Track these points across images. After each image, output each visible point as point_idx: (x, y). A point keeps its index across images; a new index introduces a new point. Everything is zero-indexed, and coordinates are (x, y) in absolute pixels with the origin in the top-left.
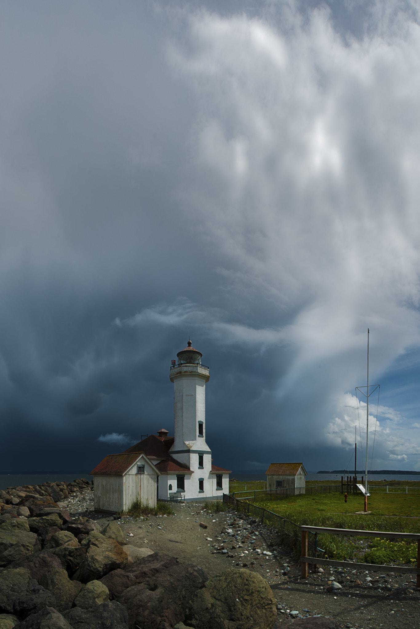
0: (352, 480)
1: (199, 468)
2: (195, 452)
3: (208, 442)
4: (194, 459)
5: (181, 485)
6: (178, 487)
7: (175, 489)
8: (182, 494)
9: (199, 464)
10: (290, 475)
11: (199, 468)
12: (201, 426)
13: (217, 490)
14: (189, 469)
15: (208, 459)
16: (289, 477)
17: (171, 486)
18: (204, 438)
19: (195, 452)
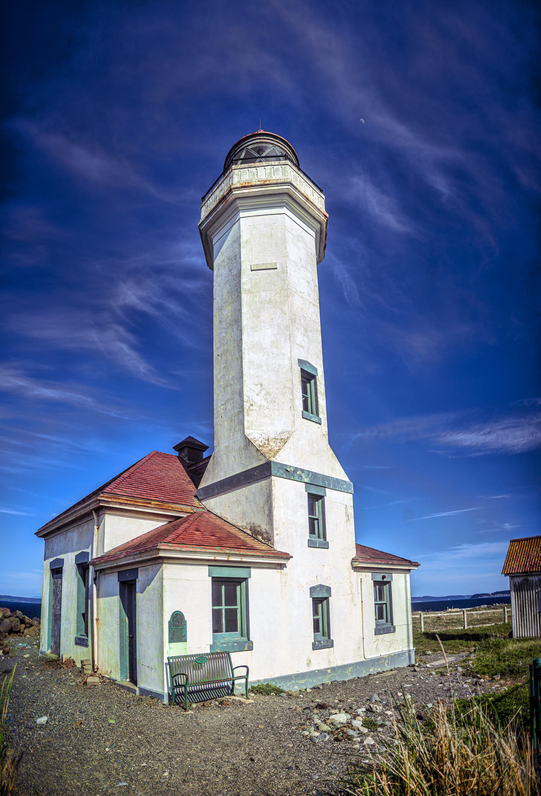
1: (311, 544)
2: (289, 473)
3: (335, 442)
6: (217, 629)
8: (237, 658)
11: (311, 544)
12: (307, 377)
15: (339, 505)
19: (289, 473)
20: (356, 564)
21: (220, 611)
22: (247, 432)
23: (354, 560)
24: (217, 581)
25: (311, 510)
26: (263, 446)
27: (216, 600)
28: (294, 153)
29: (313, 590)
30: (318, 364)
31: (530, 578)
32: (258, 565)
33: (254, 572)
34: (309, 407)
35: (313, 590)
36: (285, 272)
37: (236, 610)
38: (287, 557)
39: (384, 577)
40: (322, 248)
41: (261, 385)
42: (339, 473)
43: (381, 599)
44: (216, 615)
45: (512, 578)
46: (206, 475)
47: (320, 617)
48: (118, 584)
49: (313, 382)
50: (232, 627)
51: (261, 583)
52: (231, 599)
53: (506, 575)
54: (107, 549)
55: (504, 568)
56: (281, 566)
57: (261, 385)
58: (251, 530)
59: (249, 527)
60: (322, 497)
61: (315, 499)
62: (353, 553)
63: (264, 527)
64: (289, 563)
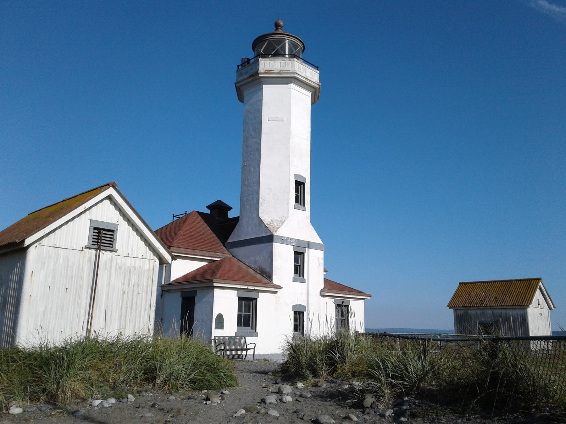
0: (97, 231)
1: (294, 280)
2: (284, 241)
3: (315, 221)
4: (282, 258)
5: (247, 316)
6: (239, 324)
7: (231, 328)
8: (249, 340)
9: (296, 272)
10: (513, 307)
11: (294, 280)
12: (299, 185)
13: (230, 208)
14: (269, 276)
15: (315, 260)
16: (500, 311)
17: (220, 318)
18: (308, 212)
19: (284, 241)
20: (323, 293)
21: (242, 315)
22: (260, 216)
23: (322, 290)
24: (241, 299)
25: (296, 260)
26: (270, 225)
27: (240, 309)
28: (301, 42)
29: (294, 307)
30: (306, 175)
31: (469, 312)
32: (273, 80)
33: (261, 294)
34: (299, 200)
35: (294, 307)
36: (289, 123)
37: (250, 315)
38: (280, 288)
39: (343, 302)
40: (316, 98)
41: (271, 189)
42: (315, 238)
43: (342, 316)
44: (239, 317)
45: (455, 310)
46: (232, 235)
47: (298, 323)
48: (181, 299)
49: (302, 186)
50: (247, 324)
51: (265, 302)
52: (248, 309)
53: (451, 308)
54: (173, 279)
55: (450, 303)
56: (276, 292)
57: (271, 189)
58: (259, 270)
59: (258, 269)
60: (303, 253)
61: (299, 256)
62: (322, 286)
63: (267, 270)
64: (280, 292)
